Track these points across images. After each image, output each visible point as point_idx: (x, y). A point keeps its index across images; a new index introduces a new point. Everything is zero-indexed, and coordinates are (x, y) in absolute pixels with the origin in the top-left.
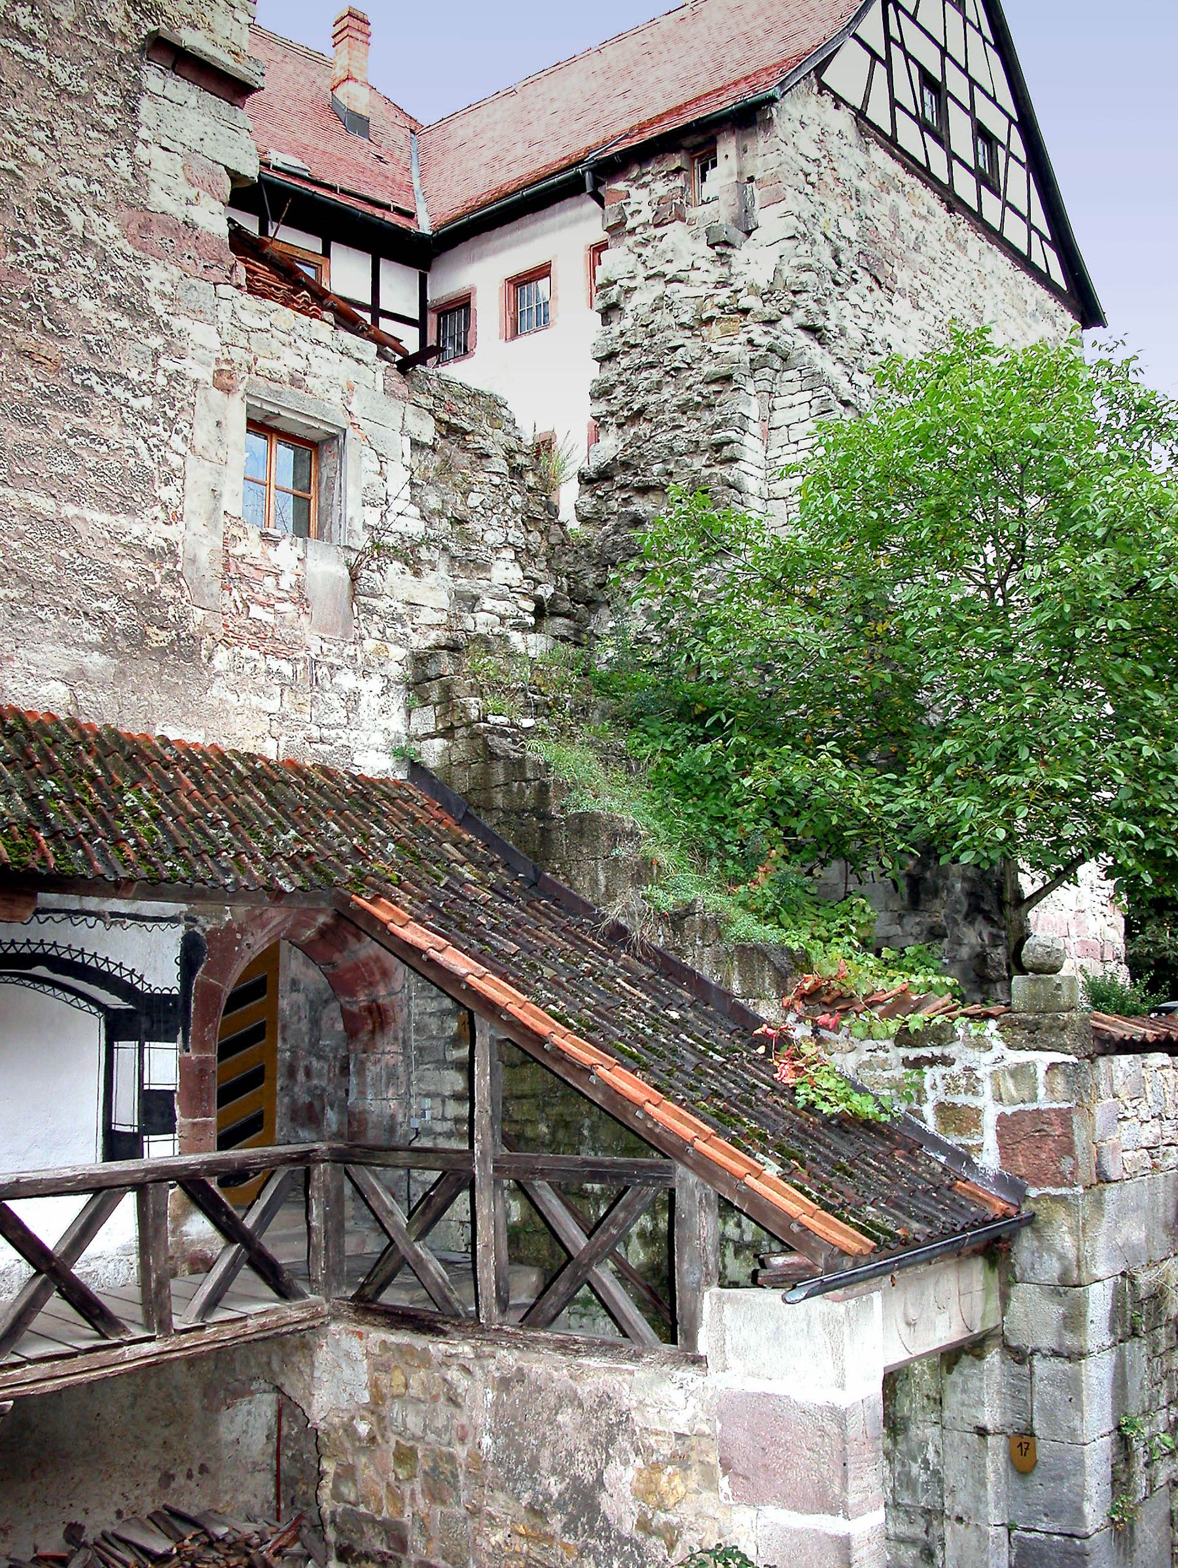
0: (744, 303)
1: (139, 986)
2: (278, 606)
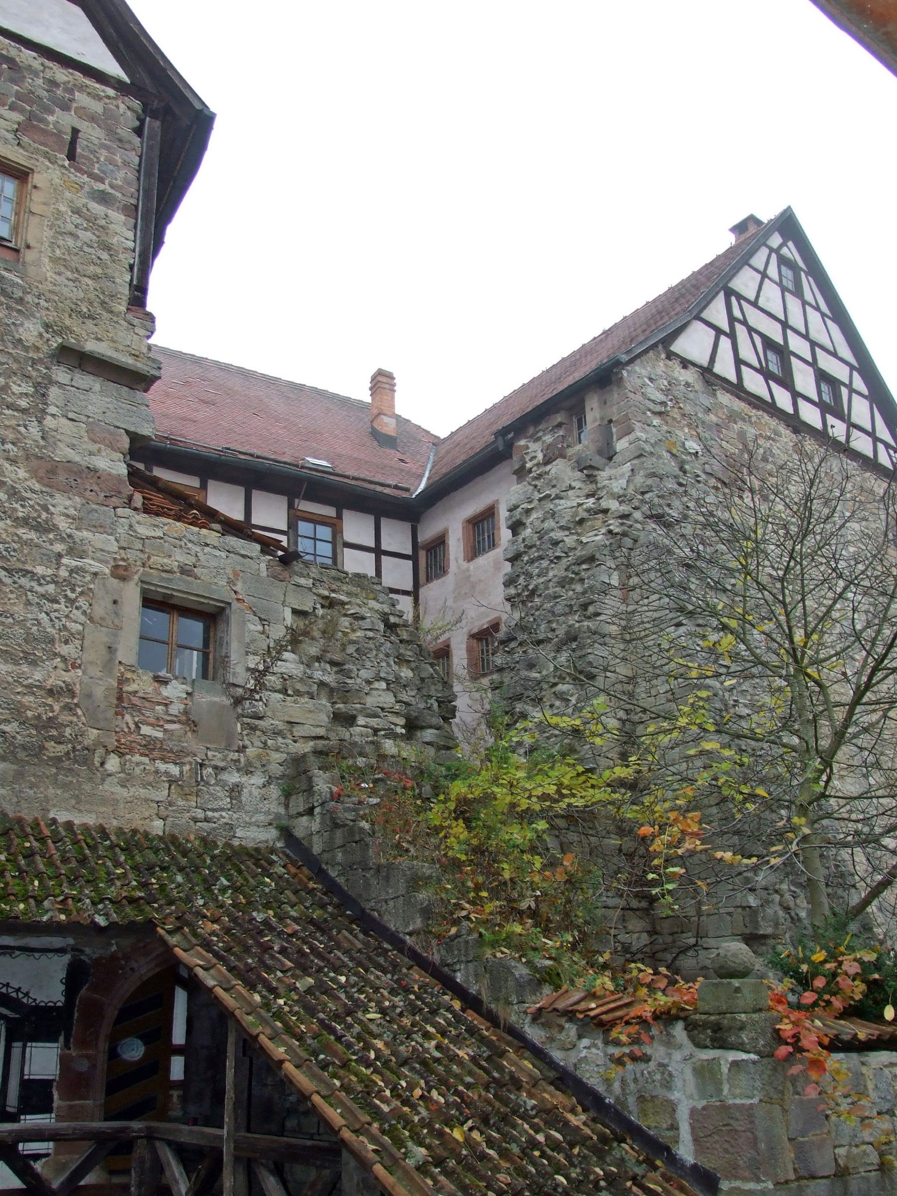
0: (604, 504)
1: (25, 1000)
2: (167, 726)
